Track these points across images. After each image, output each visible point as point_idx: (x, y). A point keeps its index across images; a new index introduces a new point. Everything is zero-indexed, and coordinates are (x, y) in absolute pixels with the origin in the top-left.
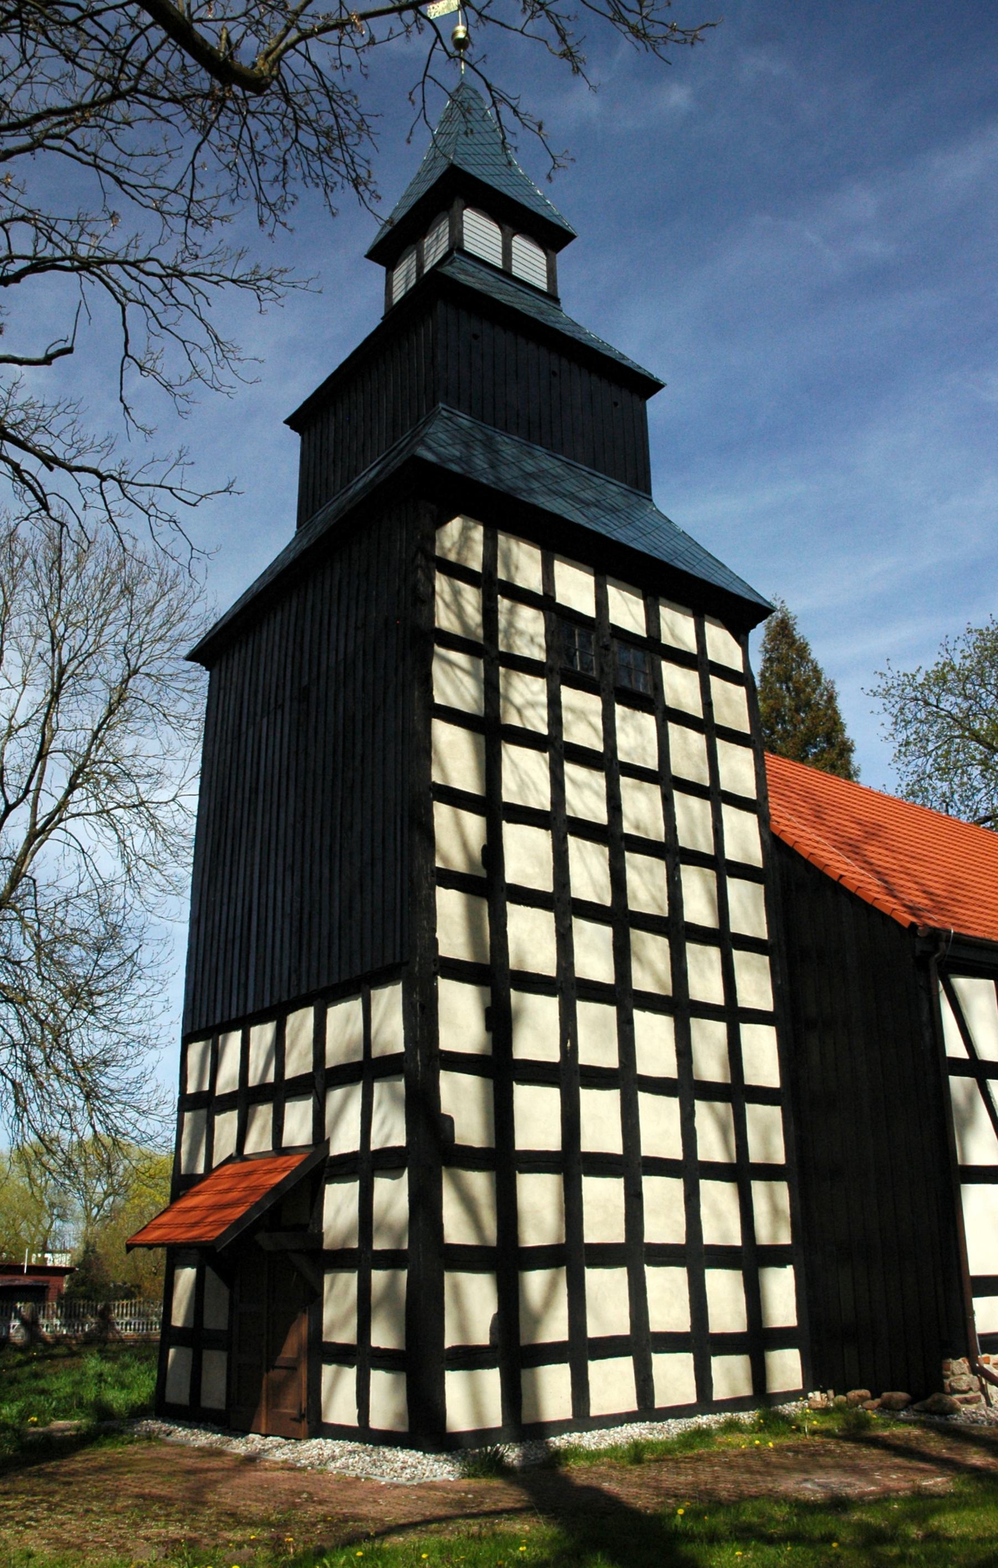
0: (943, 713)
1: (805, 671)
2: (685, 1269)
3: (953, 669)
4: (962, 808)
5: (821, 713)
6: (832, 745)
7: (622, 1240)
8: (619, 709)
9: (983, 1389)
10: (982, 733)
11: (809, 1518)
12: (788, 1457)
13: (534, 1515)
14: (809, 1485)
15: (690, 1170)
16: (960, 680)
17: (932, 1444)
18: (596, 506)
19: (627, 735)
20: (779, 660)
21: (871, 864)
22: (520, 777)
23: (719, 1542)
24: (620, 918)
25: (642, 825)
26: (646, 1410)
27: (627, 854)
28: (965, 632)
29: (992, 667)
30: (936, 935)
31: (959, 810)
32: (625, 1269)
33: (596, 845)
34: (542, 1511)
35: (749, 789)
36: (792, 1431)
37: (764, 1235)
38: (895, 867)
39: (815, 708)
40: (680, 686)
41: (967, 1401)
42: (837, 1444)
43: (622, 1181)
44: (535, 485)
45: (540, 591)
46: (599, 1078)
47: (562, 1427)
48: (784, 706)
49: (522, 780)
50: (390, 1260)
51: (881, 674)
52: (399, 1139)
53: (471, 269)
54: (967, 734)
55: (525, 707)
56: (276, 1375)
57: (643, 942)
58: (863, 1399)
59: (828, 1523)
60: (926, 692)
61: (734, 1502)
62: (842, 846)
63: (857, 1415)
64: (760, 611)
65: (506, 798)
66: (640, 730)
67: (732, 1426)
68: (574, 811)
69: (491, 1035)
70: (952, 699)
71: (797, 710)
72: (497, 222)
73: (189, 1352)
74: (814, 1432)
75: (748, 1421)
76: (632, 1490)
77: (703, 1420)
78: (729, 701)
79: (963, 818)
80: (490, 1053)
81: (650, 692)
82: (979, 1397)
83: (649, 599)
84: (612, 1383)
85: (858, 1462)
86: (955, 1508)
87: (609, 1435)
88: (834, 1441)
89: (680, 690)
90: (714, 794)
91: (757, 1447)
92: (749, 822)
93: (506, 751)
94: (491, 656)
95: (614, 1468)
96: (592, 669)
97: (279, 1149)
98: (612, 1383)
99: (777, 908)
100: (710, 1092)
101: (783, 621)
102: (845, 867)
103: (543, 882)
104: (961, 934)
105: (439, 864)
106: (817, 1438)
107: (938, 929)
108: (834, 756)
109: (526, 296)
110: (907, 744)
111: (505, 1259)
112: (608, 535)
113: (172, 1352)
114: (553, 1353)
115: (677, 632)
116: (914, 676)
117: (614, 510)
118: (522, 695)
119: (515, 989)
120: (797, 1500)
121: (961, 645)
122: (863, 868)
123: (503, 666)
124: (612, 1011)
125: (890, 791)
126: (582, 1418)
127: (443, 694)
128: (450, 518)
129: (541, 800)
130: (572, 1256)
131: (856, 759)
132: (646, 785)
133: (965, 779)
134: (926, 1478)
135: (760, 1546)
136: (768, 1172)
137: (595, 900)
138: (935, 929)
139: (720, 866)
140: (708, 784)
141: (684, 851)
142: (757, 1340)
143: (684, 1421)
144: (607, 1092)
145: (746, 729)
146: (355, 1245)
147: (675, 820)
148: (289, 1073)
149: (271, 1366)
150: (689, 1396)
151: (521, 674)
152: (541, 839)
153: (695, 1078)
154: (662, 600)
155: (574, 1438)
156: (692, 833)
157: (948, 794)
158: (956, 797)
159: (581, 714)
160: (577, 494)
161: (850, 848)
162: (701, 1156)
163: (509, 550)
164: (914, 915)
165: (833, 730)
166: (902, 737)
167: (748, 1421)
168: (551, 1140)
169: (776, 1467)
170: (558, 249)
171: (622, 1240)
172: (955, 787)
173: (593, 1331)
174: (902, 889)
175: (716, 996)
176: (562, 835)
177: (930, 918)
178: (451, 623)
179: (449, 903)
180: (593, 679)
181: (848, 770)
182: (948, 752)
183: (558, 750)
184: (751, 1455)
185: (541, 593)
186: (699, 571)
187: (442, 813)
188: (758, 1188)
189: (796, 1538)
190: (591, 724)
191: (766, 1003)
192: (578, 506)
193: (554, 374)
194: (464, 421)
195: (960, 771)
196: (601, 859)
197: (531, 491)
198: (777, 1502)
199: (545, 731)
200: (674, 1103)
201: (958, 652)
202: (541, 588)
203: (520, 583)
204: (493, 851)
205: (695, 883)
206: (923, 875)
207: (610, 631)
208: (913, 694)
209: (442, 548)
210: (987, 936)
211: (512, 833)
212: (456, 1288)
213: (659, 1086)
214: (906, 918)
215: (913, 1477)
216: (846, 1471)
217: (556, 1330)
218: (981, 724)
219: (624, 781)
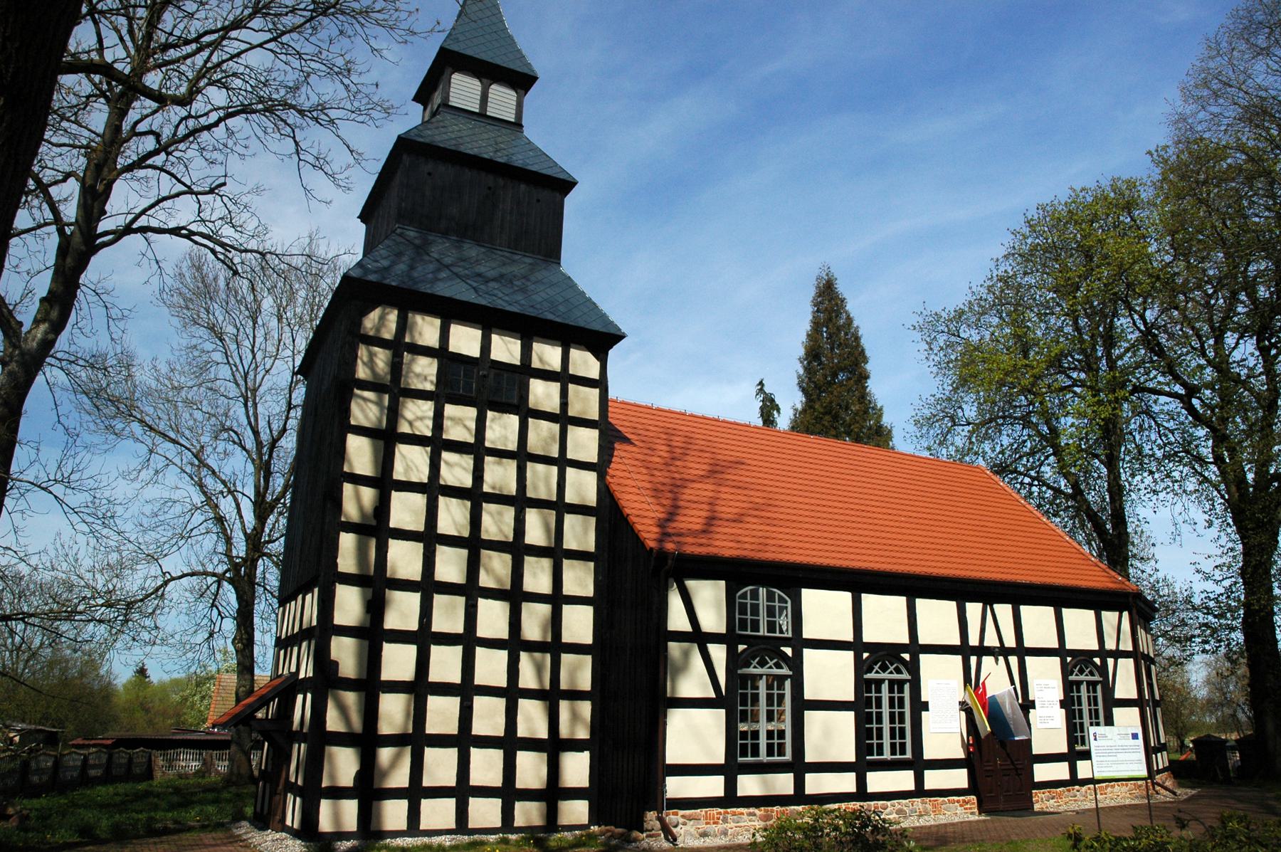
40: (543, 394)
80: (368, 625)
92: (590, 478)
98: (438, 813)
114: (397, 794)
127: (356, 419)
139: (560, 507)
142: (553, 793)
156: (535, 488)
159: (458, 421)
173: (427, 782)
179: (347, 541)
183: (437, 444)
187: (348, 488)
190: (465, 426)
192: (475, 284)
204: (382, 508)
212: (330, 756)
217: (400, 778)
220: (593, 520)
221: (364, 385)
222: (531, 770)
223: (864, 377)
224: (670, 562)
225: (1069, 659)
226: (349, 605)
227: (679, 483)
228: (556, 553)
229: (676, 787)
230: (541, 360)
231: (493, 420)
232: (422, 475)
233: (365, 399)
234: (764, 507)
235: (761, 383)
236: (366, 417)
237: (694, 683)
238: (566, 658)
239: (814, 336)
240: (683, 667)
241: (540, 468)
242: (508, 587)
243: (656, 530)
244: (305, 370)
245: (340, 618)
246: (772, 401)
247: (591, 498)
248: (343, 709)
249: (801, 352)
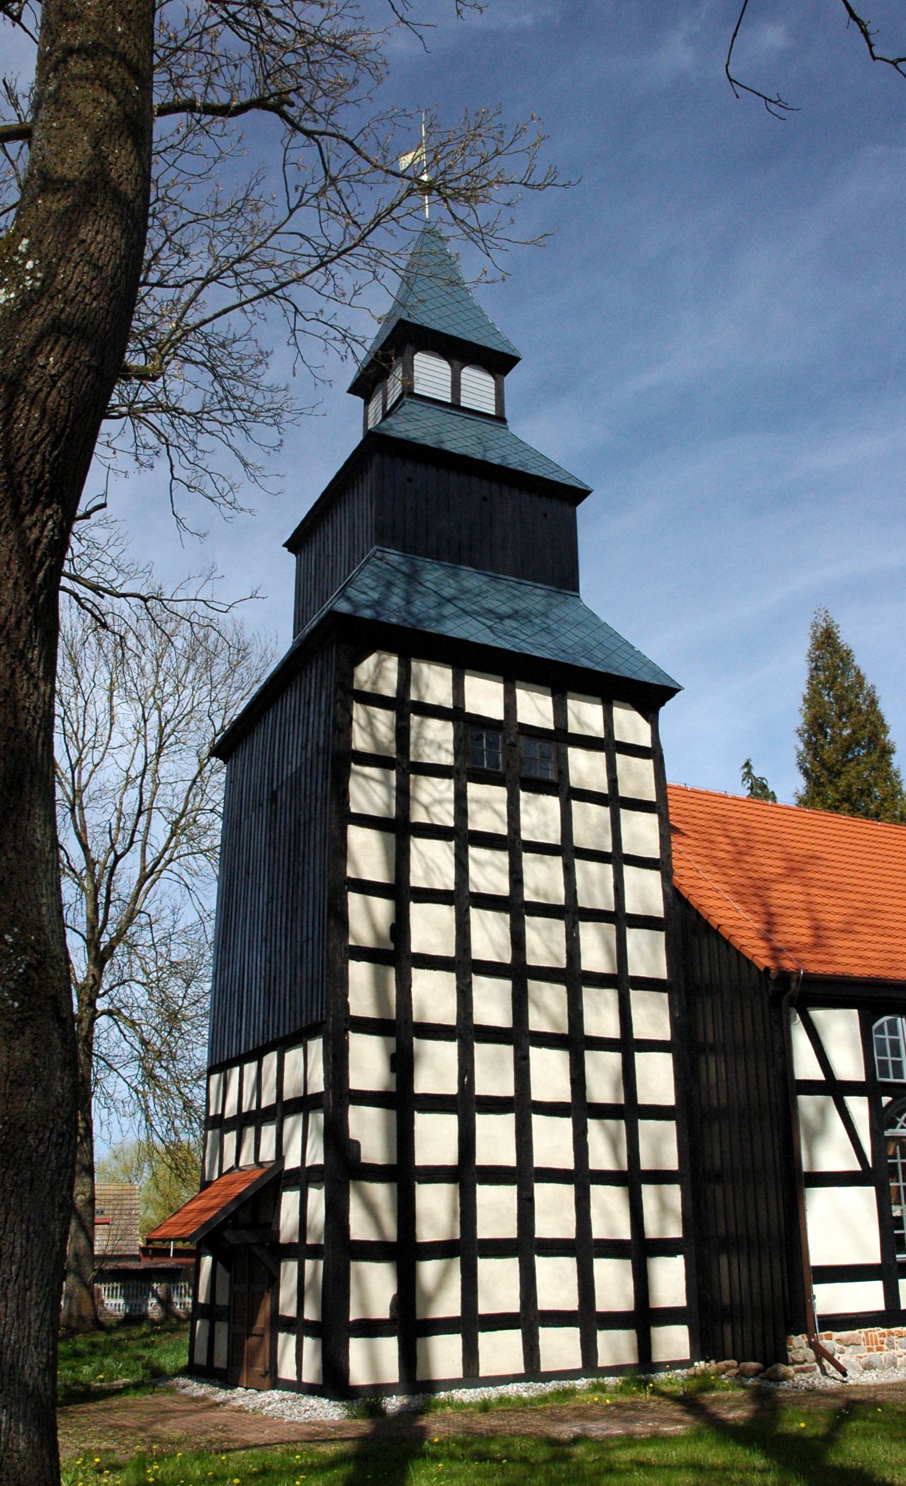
2: (574, 1259)
8: (523, 795)
25: (542, 892)
26: (532, 1370)
27: (526, 917)
30: (785, 977)
32: (517, 1259)
33: (496, 914)
37: (652, 1230)
40: (586, 769)
41: (803, 1371)
49: (427, 866)
50: (315, 1252)
52: (320, 1161)
55: (432, 804)
56: (253, 1341)
66: (543, 811)
68: (476, 887)
69: (395, 1075)
72: (446, 359)
73: (207, 1323)
80: (394, 1089)
84: (501, 1351)
92: (653, 879)
94: (402, 765)
97: (258, 1163)
98: (501, 1351)
99: (676, 953)
105: (351, 942)
111: (404, 1252)
113: (198, 1322)
114: (446, 1326)
126: (471, 1374)
127: (358, 804)
130: (466, 1248)
137: (495, 959)
139: (620, 919)
142: (643, 1317)
146: (297, 1241)
148: (263, 1105)
149: (250, 1335)
153: (588, 1100)
156: (590, 895)
159: (485, 804)
173: (484, 1308)
179: (359, 973)
180: (500, 773)
183: (462, 837)
187: (354, 900)
188: (648, 1192)
190: (495, 812)
191: (664, 1033)
192: (490, 623)
196: (502, 924)
199: (451, 823)
202: (451, 701)
203: (429, 700)
204: (400, 927)
209: (358, 681)
212: (358, 1274)
217: (449, 1305)
220: (662, 935)
221: (365, 759)
222: (613, 1284)
223: (887, 752)
224: (793, 985)
226: (368, 1064)
227: (760, 884)
228: (621, 982)
229: (828, 1299)
231: (527, 802)
232: (446, 880)
233: (366, 777)
234: (868, 913)
235: (747, 764)
236: (370, 801)
237: (833, 1152)
238: (645, 1126)
239: (813, 700)
240: (817, 1133)
241: (593, 867)
242: (566, 1031)
243: (762, 944)
244: (226, 747)
245: (357, 1082)
246: (764, 787)
247: (657, 908)
248: (370, 1208)
249: (798, 721)
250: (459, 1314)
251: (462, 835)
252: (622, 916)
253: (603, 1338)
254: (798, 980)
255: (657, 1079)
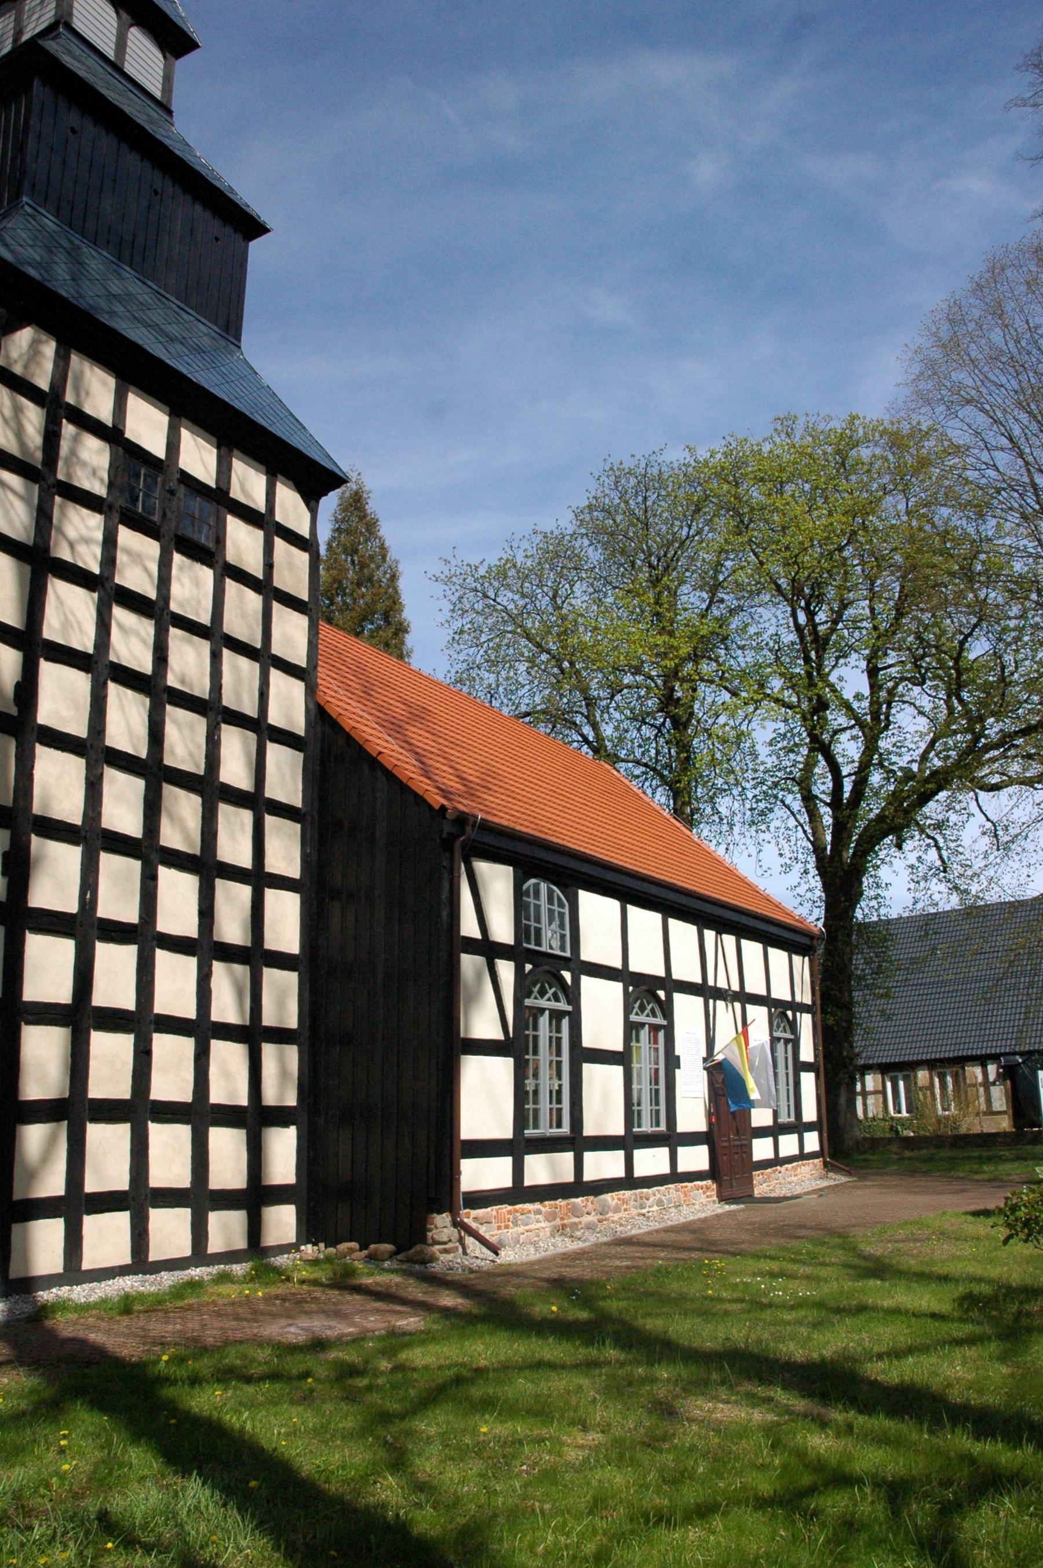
0: (499, 607)
1: (372, 547)
3: (515, 566)
4: (505, 701)
5: (382, 590)
6: (389, 623)
7: (127, 1096)
8: (177, 558)
9: (461, 1240)
10: (533, 631)
11: (289, 1358)
12: (275, 1305)
13: (14, 1368)
14: (292, 1329)
15: (202, 1030)
16: (519, 578)
17: (410, 1289)
18: (182, 343)
19: (182, 585)
20: (348, 532)
21: (410, 744)
22: (65, 614)
23: (200, 1384)
24: (154, 771)
25: (187, 680)
26: (140, 1261)
27: (168, 708)
28: (531, 532)
29: (551, 570)
30: (462, 820)
31: (502, 703)
32: (128, 1125)
33: (136, 695)
34: (22, 1364)
35: (299, 656)
36: (282, 1281)
37: (271, 1096)
38: (433, 750)
39: (377, 585)
40: (243, 543)
41: (446, 1251)
42: (323, 1292)
43: (132, 1037)
44: (119, 308)
45: (109, 423)
46: (117, 932)
47: (53, 1281)
48: (347, 578)
49: (66, 618)
51: (445, 560)
53: (78, 52)
54: (519, 630)
57: (176, 798)
58: (351, 1250)
59: (309, 1362)
60: (486, 585)
61: (219, 1347)
62: (385, 724)
63: (346, 1265)
64: (333, 480)
65: (47, 634)
66: (197, 583)
67: (224, 1278)
68: (118, 657)
70: (510, 595)
71: (359, 584)
74: (302, 1282)
75: (240, 1273)
76: (119, 1340)
77: (196, 1272)
78: (291, 566)
79: (505, 711)
81: (211, 545)
82: (457, 1248)
83: (224, 450)
84: (107, 1237)
85: (340, 1307)
86: (422, 1343)
87: (100, 1288)
88: (321, 1289)
89: (243, 547)
90: (264, 657)
91: (247, 1296)
92: (297, 689)
93: (53, 586)
95: (103, 1320)
96: (154, 514)
99: (316, 778)
100: (228, 953)
101: (356, 493)
102: (385, 744)
103: (78, 727)
104: (487, 821)
106: (304, 1287)
107: (468, 814)
108: (390, 634)
109: (138, 100)
110: (462, 632)
112: (189, 376)
114: (48, 1208)
115: (248, 487)
116: (476, 568)
117: (199, 350)
118: (76, 529)
119: (37, 835)
120: (279, 1342)
121: (525, 545)
122: (402, 747)
123: (60, 496)
124: (136, 865)
125: (440, 676)
126: (73, 1270)
128: (21, 327)
129: (84, 641)
131: (410, 640)
132: (196, 638)
133: (512, 674)
134: (402, 1318)
135: (240, 1385)
136: (280, 1036)
137: (131, 751)
138: (464, 813)
140: (259, 646)
141: (226, 710)
142: (256, 1196)
143: (176, 1273)
144: (124, 947)
145: (305, 596)
147: (221, 678)
150: (183, 1248)
151: (78, 507)
152: (80, 682)
154: (236, 452)
155: (64, 1292)
156: (238, 695)
157: (494, 686)
158: (501, 689)
159: (137, 558)
160: (162, 327)
161: (392, 727)
162: (215, 1017)
163: (82, 372)
164: (445, 797)
165: (391, 609)
166: (457, 625)
167: (240, 1273)
168: (62, 993)
169: (262, 1314)
170: (178, 56)
171: (127, 1096)
172: (501, 680)
173: (91, 1186)
174: (437, 772)
175: (244, 859)
176: (102, 680)
177: (460, 803)
178: (8, 440)
180: (154, 523)
181: (401, 650)
182: (499, 646)
184: (240, 1304)
185: (110, 425)
186: (278, 429)
189: (274, 1376)
190: (146, 570)
191: (294, 871)
193: (156, 192)
194: (50, 223)
195: (508, 665)
197: (113, 313)
198: (261, 1345)
199: (96, 570)
200: (192, 962)
201: (521, 550)
203: (88, 409)
205: (235, 745)
206: (459, 760)
207: (178, 476)
208: (474, 585)
210: (512, 825)
211: (50, 673)
213: (178, 945)
214: (437, 800)
215: (390, 1318)
216: (328, 1316)
217: (53, 1184)
218: (534, 623)
219: (174, 632)
225: (528, 967)
230: (243, 490)
242: (197, 851)
247: (299, 725)
250: (62, 1193)
251: (107, 585)
252: (264, 726)
253: (216, 1219)
254: (473, 826)
255: (285, 922)
